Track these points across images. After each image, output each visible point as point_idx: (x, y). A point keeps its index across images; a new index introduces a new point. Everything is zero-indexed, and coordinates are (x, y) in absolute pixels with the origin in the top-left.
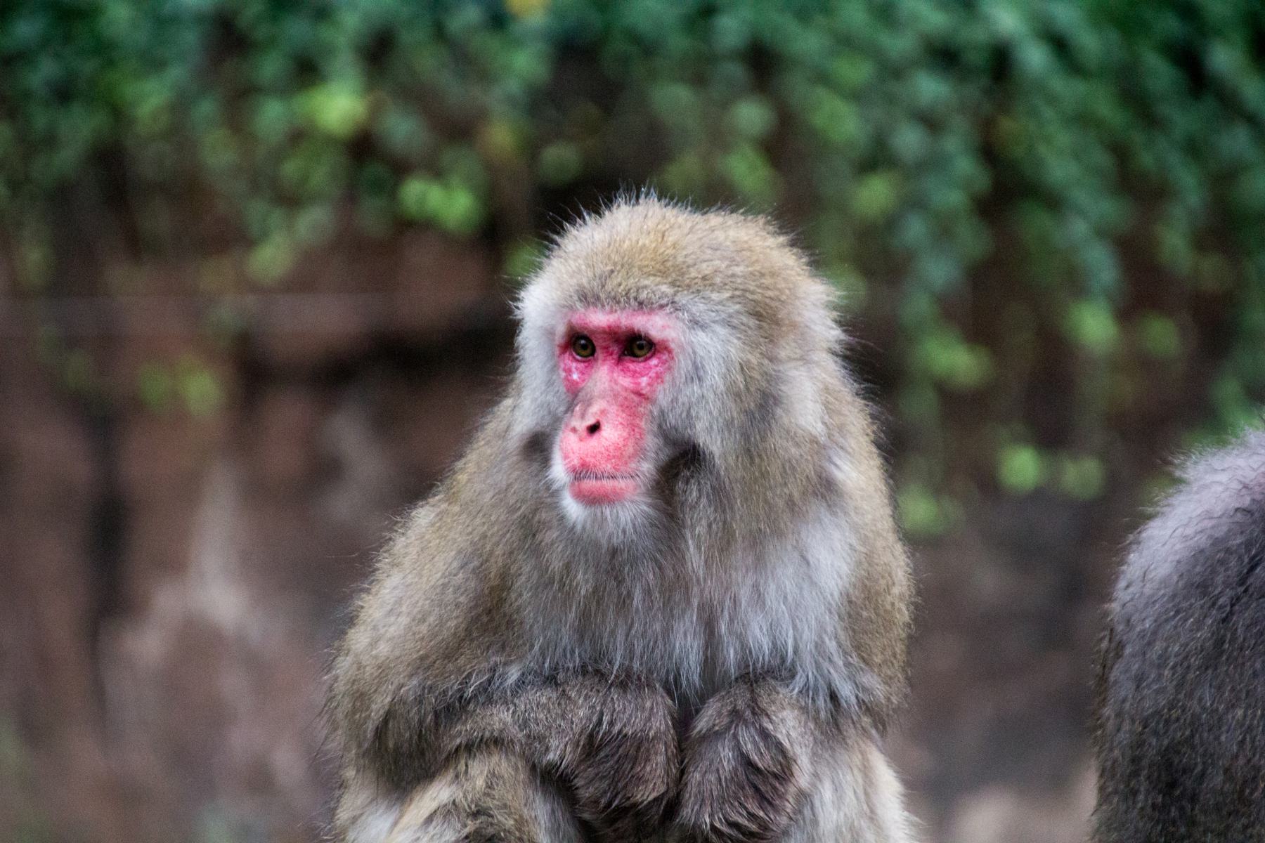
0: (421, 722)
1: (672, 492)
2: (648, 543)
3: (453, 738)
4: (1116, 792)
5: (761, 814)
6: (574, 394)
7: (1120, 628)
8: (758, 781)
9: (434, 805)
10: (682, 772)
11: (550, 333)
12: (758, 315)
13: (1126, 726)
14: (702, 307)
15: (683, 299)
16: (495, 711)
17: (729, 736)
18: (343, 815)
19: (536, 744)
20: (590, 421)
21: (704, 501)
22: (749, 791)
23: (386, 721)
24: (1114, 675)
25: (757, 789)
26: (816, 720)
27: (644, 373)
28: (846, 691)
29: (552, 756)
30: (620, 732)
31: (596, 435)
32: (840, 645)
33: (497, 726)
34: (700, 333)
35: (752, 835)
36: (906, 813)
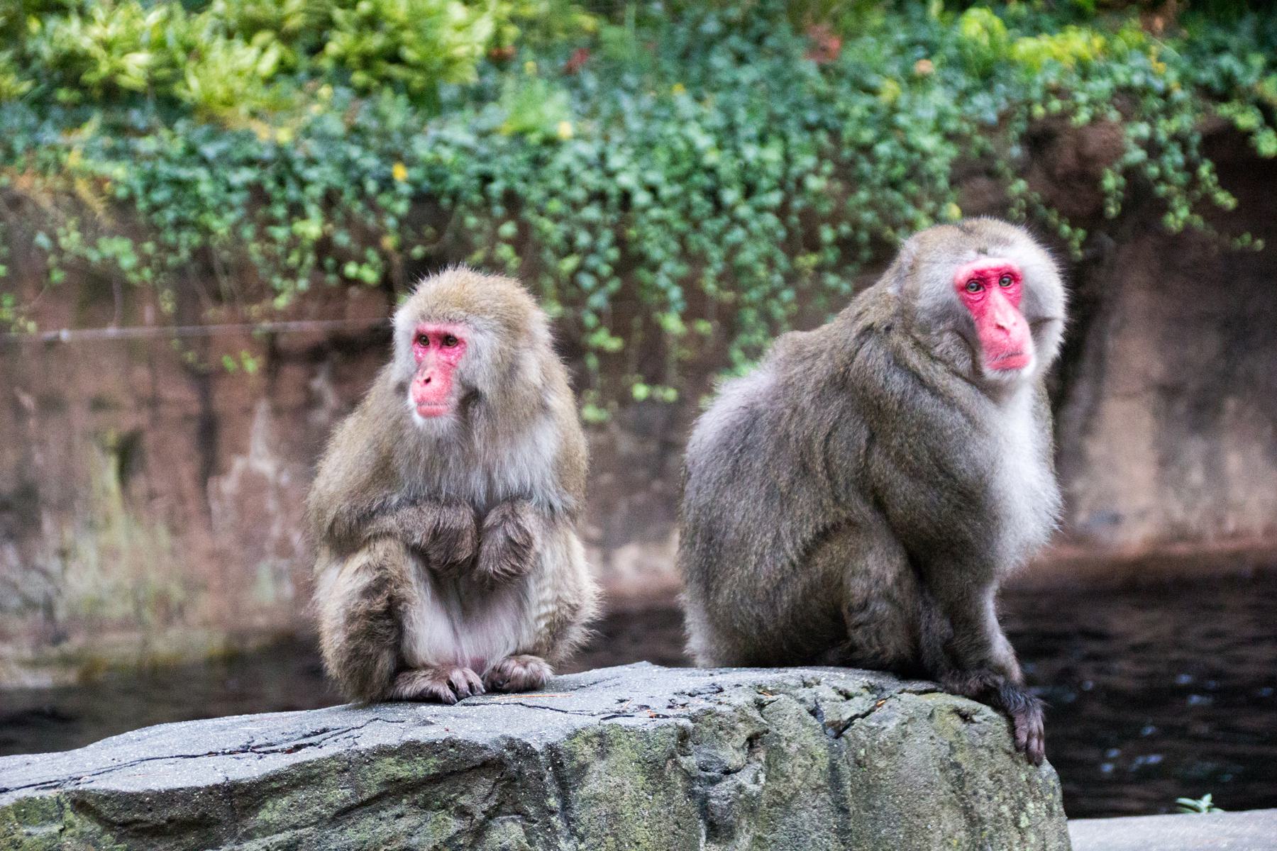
0: (351, 524)
1: (466, 412)
2: (455, 436)
3: (367, 533)
4: (686, 543)
6: (419, 361)
7: (690, 466)
9: (359, 565)
10: (480, 544)
12: (509, 327)
13: (692, 512)
14: (480, 322)
17: (501, 528)
18: (317, 568)
21: (482, 416)
22: (511, 554)
23: (333, 523)
24: (687, 488)
26: (544, 518)
27: (452, 354)
28: (557, 504)
29: (416, 541)
32: (553, 482)
35: (513, 575)
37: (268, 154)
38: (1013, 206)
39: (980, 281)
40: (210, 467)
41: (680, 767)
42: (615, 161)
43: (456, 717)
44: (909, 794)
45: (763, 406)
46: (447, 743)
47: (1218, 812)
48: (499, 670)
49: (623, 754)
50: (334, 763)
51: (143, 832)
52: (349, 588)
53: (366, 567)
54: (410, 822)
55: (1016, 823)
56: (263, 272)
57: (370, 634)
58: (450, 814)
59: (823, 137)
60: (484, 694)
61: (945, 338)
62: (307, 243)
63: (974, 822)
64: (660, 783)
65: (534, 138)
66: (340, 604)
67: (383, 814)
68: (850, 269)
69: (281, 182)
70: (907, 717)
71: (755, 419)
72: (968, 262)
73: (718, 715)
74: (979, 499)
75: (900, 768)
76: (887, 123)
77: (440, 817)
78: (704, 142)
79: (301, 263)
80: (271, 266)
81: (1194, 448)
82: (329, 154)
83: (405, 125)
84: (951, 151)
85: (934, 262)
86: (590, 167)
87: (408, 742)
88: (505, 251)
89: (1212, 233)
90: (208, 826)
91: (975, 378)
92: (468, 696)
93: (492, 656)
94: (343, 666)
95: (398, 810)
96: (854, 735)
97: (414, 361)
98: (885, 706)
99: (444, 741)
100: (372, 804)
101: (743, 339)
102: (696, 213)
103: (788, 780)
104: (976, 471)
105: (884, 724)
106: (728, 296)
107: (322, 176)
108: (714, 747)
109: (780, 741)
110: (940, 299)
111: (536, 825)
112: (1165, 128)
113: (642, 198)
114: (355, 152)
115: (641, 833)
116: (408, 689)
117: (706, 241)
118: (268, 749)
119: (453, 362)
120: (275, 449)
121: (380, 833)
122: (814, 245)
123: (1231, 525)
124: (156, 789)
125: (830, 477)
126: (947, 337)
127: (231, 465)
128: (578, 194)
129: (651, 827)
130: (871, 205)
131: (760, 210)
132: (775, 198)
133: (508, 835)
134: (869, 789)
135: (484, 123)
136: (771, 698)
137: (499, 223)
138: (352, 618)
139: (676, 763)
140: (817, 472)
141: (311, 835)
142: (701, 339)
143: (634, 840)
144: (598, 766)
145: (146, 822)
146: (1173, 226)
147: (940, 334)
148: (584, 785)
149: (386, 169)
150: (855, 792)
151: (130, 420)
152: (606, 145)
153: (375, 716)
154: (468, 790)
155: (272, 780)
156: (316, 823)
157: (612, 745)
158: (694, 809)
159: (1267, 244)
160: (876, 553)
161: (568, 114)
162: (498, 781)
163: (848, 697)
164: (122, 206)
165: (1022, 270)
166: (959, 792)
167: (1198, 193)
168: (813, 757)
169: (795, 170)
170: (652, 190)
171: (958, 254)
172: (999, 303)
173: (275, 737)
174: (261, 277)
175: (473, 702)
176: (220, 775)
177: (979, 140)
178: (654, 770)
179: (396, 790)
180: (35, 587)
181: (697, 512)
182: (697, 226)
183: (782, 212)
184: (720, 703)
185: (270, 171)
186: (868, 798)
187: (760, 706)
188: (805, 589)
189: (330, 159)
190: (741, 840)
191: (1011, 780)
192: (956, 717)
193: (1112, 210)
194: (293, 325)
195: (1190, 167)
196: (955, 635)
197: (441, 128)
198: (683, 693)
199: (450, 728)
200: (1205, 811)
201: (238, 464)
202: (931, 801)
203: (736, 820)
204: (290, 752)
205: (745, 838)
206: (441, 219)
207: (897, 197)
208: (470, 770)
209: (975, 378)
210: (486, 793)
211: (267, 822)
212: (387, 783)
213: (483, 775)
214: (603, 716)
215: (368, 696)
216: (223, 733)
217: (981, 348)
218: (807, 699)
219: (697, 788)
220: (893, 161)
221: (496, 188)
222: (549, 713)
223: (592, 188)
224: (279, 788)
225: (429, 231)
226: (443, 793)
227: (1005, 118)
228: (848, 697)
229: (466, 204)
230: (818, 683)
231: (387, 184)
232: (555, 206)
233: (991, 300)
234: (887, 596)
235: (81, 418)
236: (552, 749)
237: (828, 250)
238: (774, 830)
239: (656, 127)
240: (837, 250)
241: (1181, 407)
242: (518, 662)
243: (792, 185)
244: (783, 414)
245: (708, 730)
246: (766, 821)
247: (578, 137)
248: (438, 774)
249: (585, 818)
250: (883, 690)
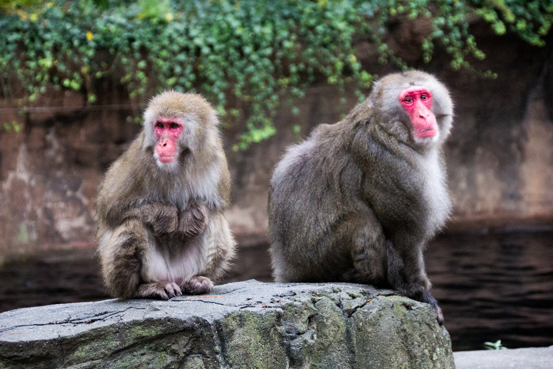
5: (197, 229)
6: (159, 137)
7: (273, 185)
8: (197, 221)
9: (121, 232)
11: (152, 123)
12: (202, 118)
14: (190, 116)
15: (185, 114)
16: (136, 210)
19: (145, 218)
20: (164, 143)
25: (196, 223)
27: (176, 132)
28: (218, 204)
30: (165, 215)
31: (165, 146)
33: (136, 213)
34: (189, 122)
35: (195, 234)
36: (230, 230)
37: (26, 26)
38: (381, 56)
39: (411, 97)
41: (277, 331)
42: (193, 32)
43: (170, 307)
44: (383, 344)
45: (309, 155)
46: (167, 319)
47: (504, 349)
48: (189, 283)
49: (251, 325)
50: (111, 329)
51: (18, 361)
52: (116, 243)
53: (125, 233)
54: (148, 357)
55: (431, 358)
56: (24, 83)
57: (127, 266)
58: (167, 354)
59: (291, 22)
60: (181, 295)
61: (395, 124)
62: (45, 69)
64: (268, 339)
65: (155, 21)
66: (112, 251)
67: (135, 353)
68: (304, 85)
69: (32, 40)
70: (381, 307)
71: (306, 162)
72: (406, 88)
73: (295, 306)
74: (417, 201)
75: (378, 332)
76: (321, 16)
77: (163, 355)
78: (235, 24)
79: (42, 79)
80: (28, 80)
81: (462, 172)
82: (56, 26)
83: (92, 13)
84: (352, 30)
85: (389, 89)
86: (181, 35)
87: (148, 319)
88: (141, 75)
89: (473, 69)
90: (50, 359)
91: (410, 143)
92: (174, 296)
93: (185, 276)
94: (112, 282)
95: (142, 352)
96: (357, 316)
97: (155, 136)
98: (371, 302)
99: (165, 318)
100: (130, 349)
101: (254, 118)
102: (232, 58)
103: (327, 337)
104: (415, 188)
105: (371, 311)
106: (246, 98)
107: (52, 37)
108: (293, 322)
109: (323, 319)
110: (393, 105)
111: (209, 359)
112: (452, 20)
113: (206, 50)
114: (68, 26)
115: (259, 363)
116: (145, 293)
117: (236, 72)
118: (78, 322)
119: (176, 136)
120: (28, 168)
121: (134, 363)
122: (287, 74)
123: (479, 207)
124: (25, 341)
125: (342, 192)
126: (396, 124)
127: (8, 176)
128: (175, 48)
129: (263, 360)
130: (314, 55)
131: (262, 57)
132: (269, 51)
133: (196, 364)
134: (364, 342)
135: (130, 13)
136: (319, 298)
137: (137, 61)
138: (117, 258)
139: (275, 330)
140: (335, 189)
141: (100, 363)
142: (233, 118)
143: (255, 367)
144: (239, 331)
145: (20, 357)
146: (456, 67)
147: (393, 122)
148: (232, 340)
149: (83, 34)
150: (357, 344)
152: (189, 24)
153: (130, 306)
154: (176, 342)
155: (81, 336)
156: (103, 358)
157: (246, 321)
158: (283, 352)
159: (499, 75)
160: (368, 226)
161: (170, 9)
162: (191, 338)
163: (354, 297)
165: (431, 91)
166: (406, 343)
167: (466, 51)
168: (338, 326)
169: (278, 38)
170: (211, 46)
171: (400, 85)
172: (421, 108)
173: (82, 316)
174: (23, 85)
175: (177, 299)
176: (56, 334)
177: (365, 24)
178: (265, 333)
179: (142, 342)
181: (277, 206)
182: (232, 64)
183: (272, 58)
184: (295, 301)
185: (27, 34)
186: (363, 346)
187: (314, 302)
188: (333, 244)
189: (56, 29)
190: (306, 367)
191: (429, 337)
192: (404, 307)
193: (427, 59)
194: (38, 109)
195: (463, 39)
196: (405, 266)
197: (110, 15)
198: (277, 296)
199: (168, 313)
200: (498, 349)
201: (11, 175)
202: (392, 347)
203: (303, 357)
204: (89, 323)
205: (307, 365)
206: (110, 59)
207: (326, 51)
208: (177, 332)
209: (410, 143)
210: (185, 344)
211: (78, 357)
212: (137, 338)
213: (184, 335)
214: (241, 307)
215: (125, 296)
216: (54, 313)
217: (413, 128)
218: (336, 298)
219: (285, 341)
220: (324, 34)
221: (136, 44)
222: (215, 305)
223: (182, 45)
224: (85, 341)
225: (104, 65)
226: (164, 344)
227: (377, 14)
228: (354, 297)
229: (122, 51)
230: (340, 291)
231: (84, 41)
232: (164, 53)
233: (417, 105)
234: (373, 247)
236: (217, 322)
237: (294, 76)
238: (320, 362)
239: (212, 17)
240: (298, 76)
241: (456, 152)
242: (198, 280)
243: (277, 45)
244: (319, 160)
245: (290, 313)
246: (317, 357)
247: (176, 20)
248: (162, 335)
249: (232, 356)
250: (369, 294)
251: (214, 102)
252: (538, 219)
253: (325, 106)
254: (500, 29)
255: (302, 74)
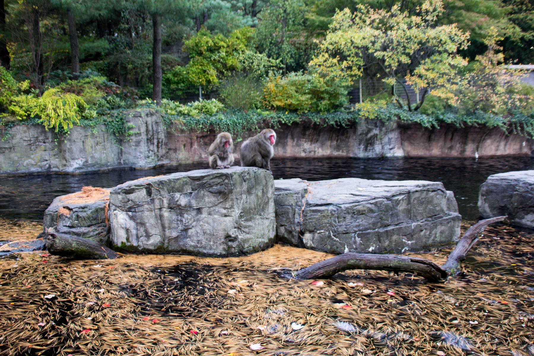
13: (317, 164)
40: (191, 147)
49: (237, 174)
63: (266, 181)
76: (251, 119)
81: (276, 148)
107: (202, 122)
134: (258, 178)
151: (185, 142)
164: (185, 124)
178: (239, 176)
179: (216, 177)
180: (176, 157)
206: (212, 126)
235: (181, 142)
243: (243, 124)
251: (231, 134)
252: (289, 157)
253: (252, 135)
254: (283, 122)
255: (247, 129)
